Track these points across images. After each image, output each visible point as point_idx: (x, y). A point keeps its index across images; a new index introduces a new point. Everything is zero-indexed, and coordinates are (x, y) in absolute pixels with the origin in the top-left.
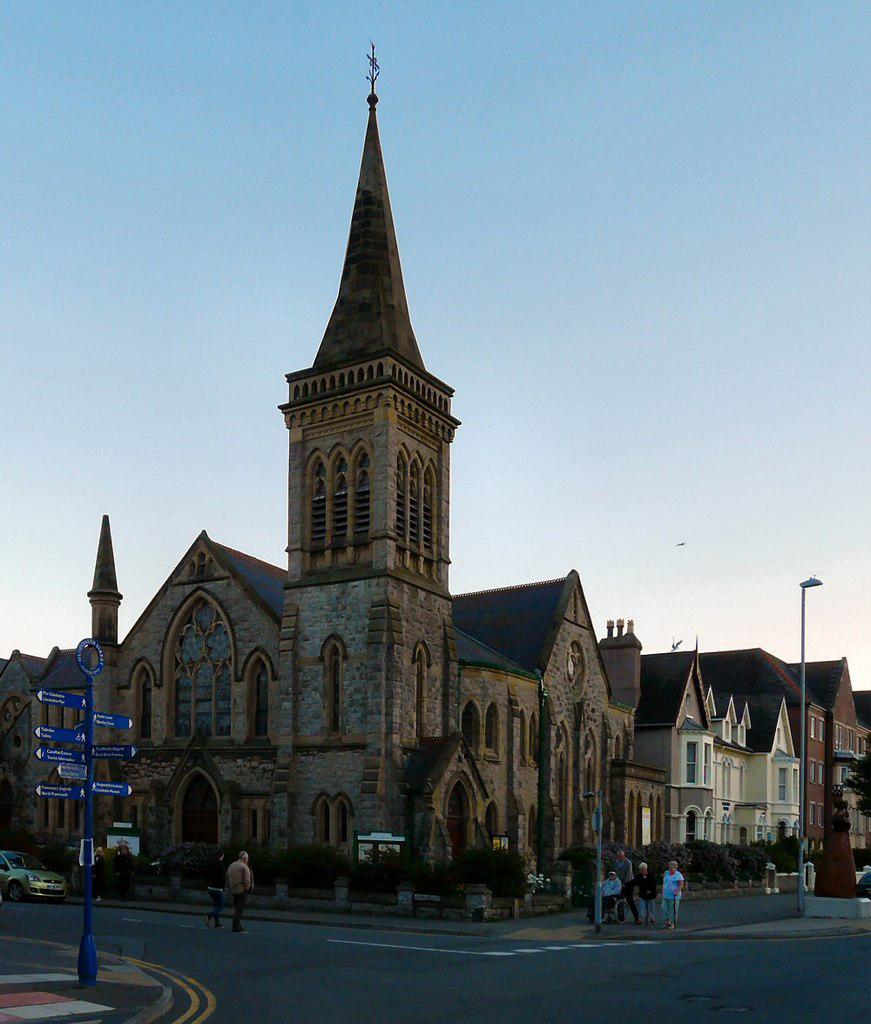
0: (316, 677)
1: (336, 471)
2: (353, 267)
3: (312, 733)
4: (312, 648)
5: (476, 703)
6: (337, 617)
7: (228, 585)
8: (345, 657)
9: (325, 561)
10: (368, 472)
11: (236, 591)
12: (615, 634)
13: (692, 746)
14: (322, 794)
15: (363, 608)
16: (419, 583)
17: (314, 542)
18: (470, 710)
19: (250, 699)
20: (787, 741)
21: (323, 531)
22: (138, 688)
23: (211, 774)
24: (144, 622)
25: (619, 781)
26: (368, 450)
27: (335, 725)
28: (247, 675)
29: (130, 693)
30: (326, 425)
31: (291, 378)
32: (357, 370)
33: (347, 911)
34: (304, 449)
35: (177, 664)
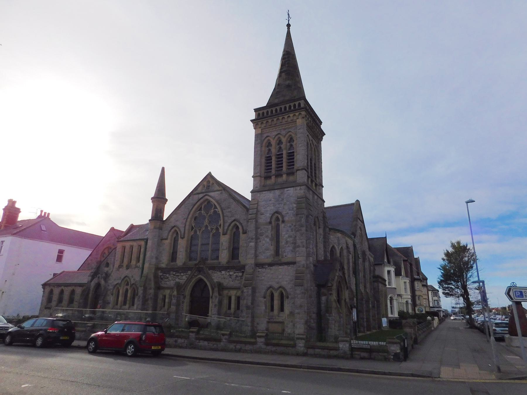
3: (266, 256)
6: (279, 204)
7: (221, 193)
8: (283, 222)
14: (270, 287)
27: (277, 253)
31: (256, 110)
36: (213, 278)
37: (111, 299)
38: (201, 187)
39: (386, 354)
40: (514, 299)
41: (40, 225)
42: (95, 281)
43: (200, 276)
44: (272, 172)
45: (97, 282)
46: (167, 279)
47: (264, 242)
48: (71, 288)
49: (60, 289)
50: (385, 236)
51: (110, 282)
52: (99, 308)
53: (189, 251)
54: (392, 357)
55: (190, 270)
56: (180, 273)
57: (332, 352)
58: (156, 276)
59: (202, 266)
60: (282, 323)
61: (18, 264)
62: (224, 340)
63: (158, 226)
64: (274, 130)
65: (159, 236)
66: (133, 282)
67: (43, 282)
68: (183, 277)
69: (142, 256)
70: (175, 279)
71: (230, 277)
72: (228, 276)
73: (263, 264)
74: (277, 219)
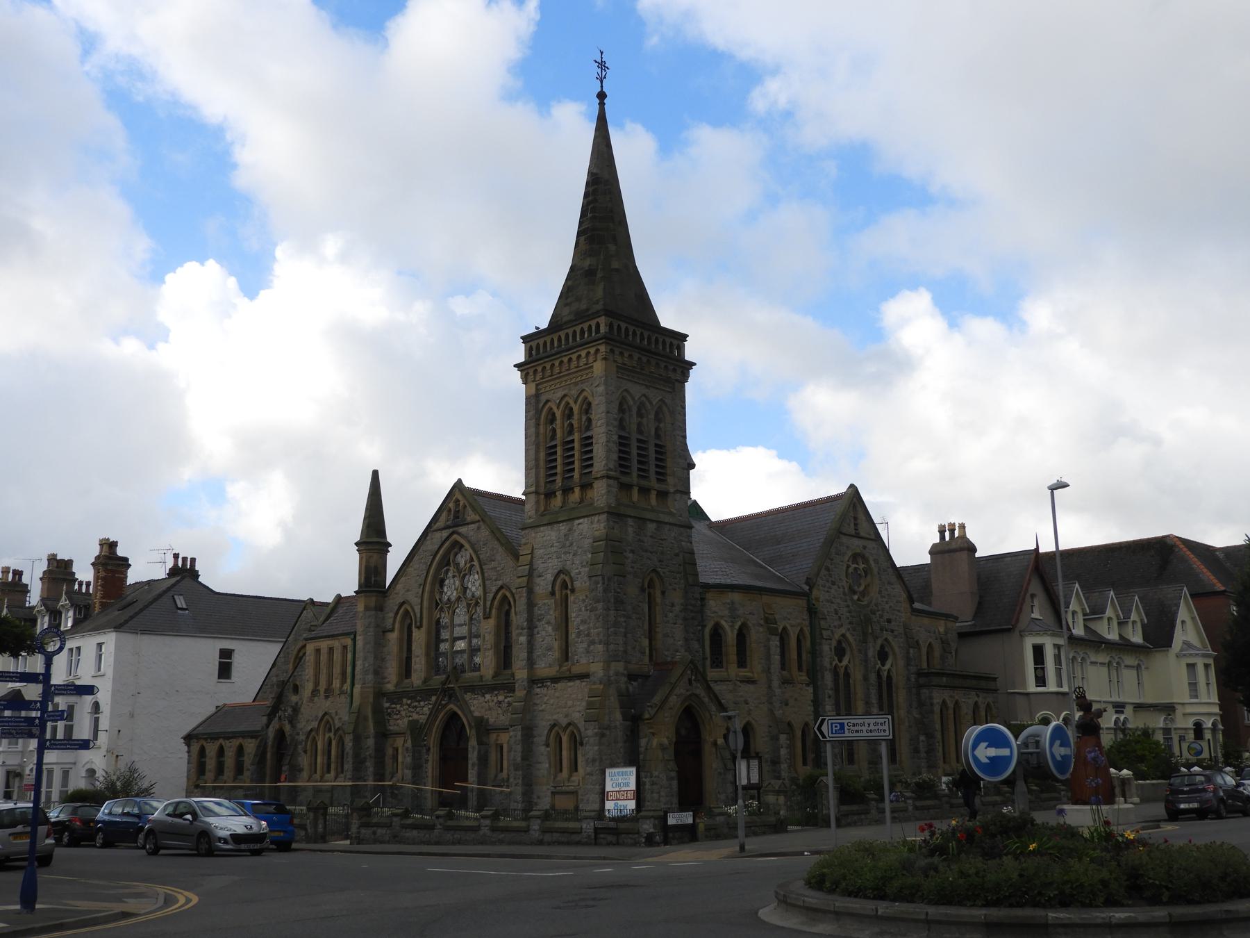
0: (547, 608)
1: (565, 419)
2: (582, 238)
3: (545, 667)
4: (543, 585)
5: (723, 623)
6: (565, 553)
7: (479, 528)
8: (573, 591)
9: (558, 501)
10: (592, 418)
11: (485, 533)
12: (947, 538)
13: (1038, 651)
14: (554, 726)
15: (587, 543)
16: (648, 515)
17: (548, 485)
18: (717, 634)
19: (497, 634)
20: (1198, 632)
21: (555, 474)
22: (498, 617)
23: (463, 712)
24: (407, 567)
25: (927, 691)
26: (590, 399)
27: (566, 655)
28: (494, 612)
29: (393, 636)
30: (555, 379)
31: (526, 339)
32: (550, 339)
33: (541, 843)
34: (538, 402)
35: (437, 604)
36: (472, 709)
37: (304, 761)
38: (444, 514)
39: (636, 836)
40: (827, 736)
41: (173, 596)
42: (275, 724)
43: (451, 706)
44: (557, 481)
45: (277, 727)
46: (397, 714)
47: (544, 633)
48: (236, 742)
49: (217, 743)
50: (1034, 547)
51: (299, 726)
52: (283, 782)
53: (433, 654)
54: (644, 840)
55: (434, 695)
56: (419, 701)
57: (576, 838)
58: (379, 713)
59: (452, 686)
60: (575, 793)
61: (139, 693)
62: (439, 827)
63: (373, 604)
64: (558, 386)
65: (378, 626)
66: (338, 724)
67: (185, 733)
68: (424, 709)
69: (349, 669)
70: (411, 714)
71: (499, 707)
72: (496, 703)
73: (542, 679)
74: (564, 585)
